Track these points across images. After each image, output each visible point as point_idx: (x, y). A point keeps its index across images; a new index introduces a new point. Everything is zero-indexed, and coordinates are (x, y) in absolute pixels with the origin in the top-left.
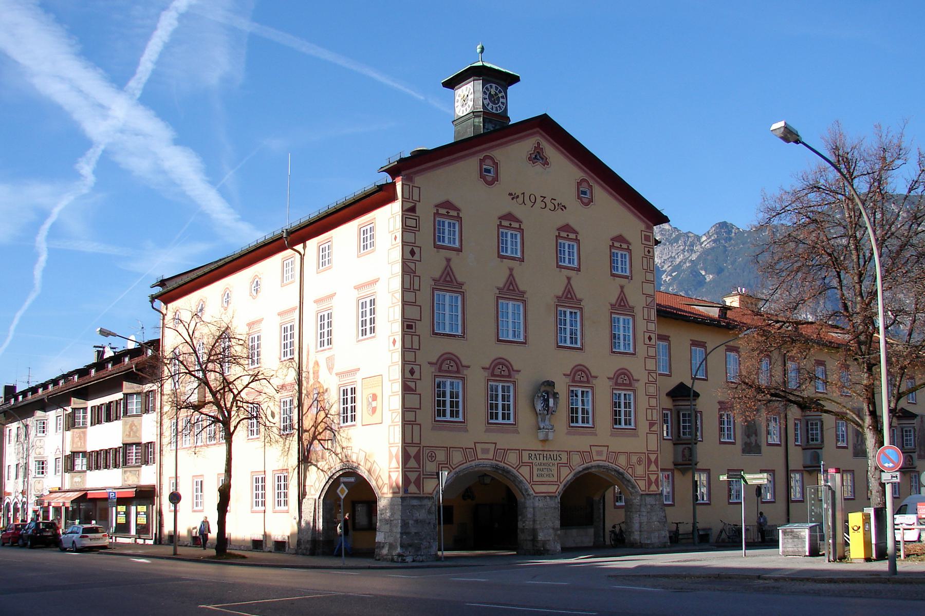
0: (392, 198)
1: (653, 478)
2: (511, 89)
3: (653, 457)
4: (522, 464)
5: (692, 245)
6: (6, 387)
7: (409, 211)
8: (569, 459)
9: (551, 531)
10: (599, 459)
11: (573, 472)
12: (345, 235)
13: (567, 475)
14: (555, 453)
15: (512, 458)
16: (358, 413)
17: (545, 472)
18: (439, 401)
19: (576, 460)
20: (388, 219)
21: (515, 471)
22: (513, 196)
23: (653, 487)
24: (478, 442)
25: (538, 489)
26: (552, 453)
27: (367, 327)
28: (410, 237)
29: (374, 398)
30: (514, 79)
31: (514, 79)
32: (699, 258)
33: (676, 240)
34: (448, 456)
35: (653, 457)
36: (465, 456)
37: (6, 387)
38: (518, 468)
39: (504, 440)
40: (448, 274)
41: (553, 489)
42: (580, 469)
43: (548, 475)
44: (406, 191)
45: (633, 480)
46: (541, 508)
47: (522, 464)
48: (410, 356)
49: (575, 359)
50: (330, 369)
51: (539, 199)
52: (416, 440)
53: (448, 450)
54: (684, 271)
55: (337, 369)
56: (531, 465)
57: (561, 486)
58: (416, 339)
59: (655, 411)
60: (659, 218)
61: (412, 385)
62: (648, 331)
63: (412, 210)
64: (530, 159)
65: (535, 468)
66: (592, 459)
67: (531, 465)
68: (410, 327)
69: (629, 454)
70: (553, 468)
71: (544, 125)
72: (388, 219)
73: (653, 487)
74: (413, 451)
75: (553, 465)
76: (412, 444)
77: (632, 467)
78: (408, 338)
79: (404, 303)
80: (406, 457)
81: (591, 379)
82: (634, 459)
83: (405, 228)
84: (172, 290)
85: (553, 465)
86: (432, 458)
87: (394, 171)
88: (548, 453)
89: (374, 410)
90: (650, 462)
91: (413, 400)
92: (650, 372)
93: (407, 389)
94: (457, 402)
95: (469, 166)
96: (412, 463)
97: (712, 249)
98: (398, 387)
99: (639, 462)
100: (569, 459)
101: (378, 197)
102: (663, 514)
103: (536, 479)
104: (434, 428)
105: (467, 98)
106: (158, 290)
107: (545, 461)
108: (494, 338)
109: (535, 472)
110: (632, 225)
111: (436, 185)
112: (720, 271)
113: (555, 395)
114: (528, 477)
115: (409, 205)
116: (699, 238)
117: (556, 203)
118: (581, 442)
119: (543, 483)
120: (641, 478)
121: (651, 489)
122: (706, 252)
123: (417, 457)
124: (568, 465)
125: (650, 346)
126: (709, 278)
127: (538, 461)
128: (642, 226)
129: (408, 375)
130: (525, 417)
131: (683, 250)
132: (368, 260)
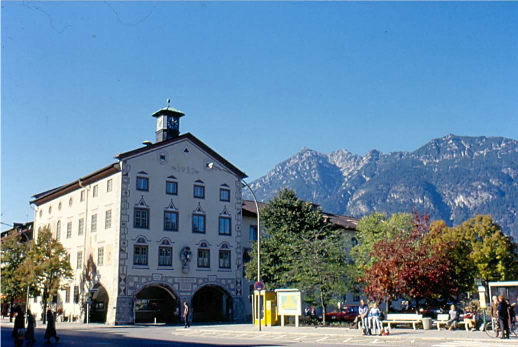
0: (117, 171)
2: (181, 119)
3: (239, 281)
5: (358, 162)
7: (125, 175)
10: (212, 281)
12: (102, 183)
13: (196, 288)
16: (104, 262)
19: (201, 281)
20: (117, 178)
22: (174, 168)
23: (239, 294)
24: (153, 273)
27: (108, 224)
28: (125, 186)
29: (110, 254)
30: (182, 115)
31: (182, 115)
32: (362, 168)
33: (350, 159)
34: (197, 281)
35: (239, 281)
39: (166, 273)
41: (189, 294)
44: (124, 167)
45: (229, 291)
48: (123, 237)
49: (199, 238)
50: (96, 240)
51: (186, 169)
54: (354, 176)
55: (98, 241)
57: (193, 294)
58: (126, 230)
59: (240, 261)
60: (242, 175)
61: (124, 249)
62: (237, 225)
63: (127, 175)
66: (208, 282)
68: (123, 224)
69: (226, 280)
71: (189, 136)
72: (117, 178)
73: (239, 294)
74: (123, 278)
76: (123, 274)
77: (229, 285)
78: (122, 229)
79: (121, 214)
80: (120, 280)
83: (123, 182)
84: (41, 199)
87: (120, 157)
89: (109, 259)
90: (237, 283)
91: (124, 256)
92: (238, 243)
93: (121, 251)
95: (154, 154)
96: (122, 282)
97: (369, 164)
98: (117, 250)
99: (232, 283)
101: (109, 171)
103: (181, 290)
105: (161, 123)
106: (34, 199)
110: (231, 179)
111: (137, 165)
112: (373, 175)
113: (190, 253)
114: (177, 289)
115: (124, 173)
116: (362, 158)
117: (194, 170)
118: (204, 274)
120: (233, 290)
122: (366, 166)
123: (125, 280)
125: (238, 231)
126: (368, 179)
128: (237, 179)
129: (122, 245)
130: (176, 262)
131: (354, 165)
132: (108, 196)
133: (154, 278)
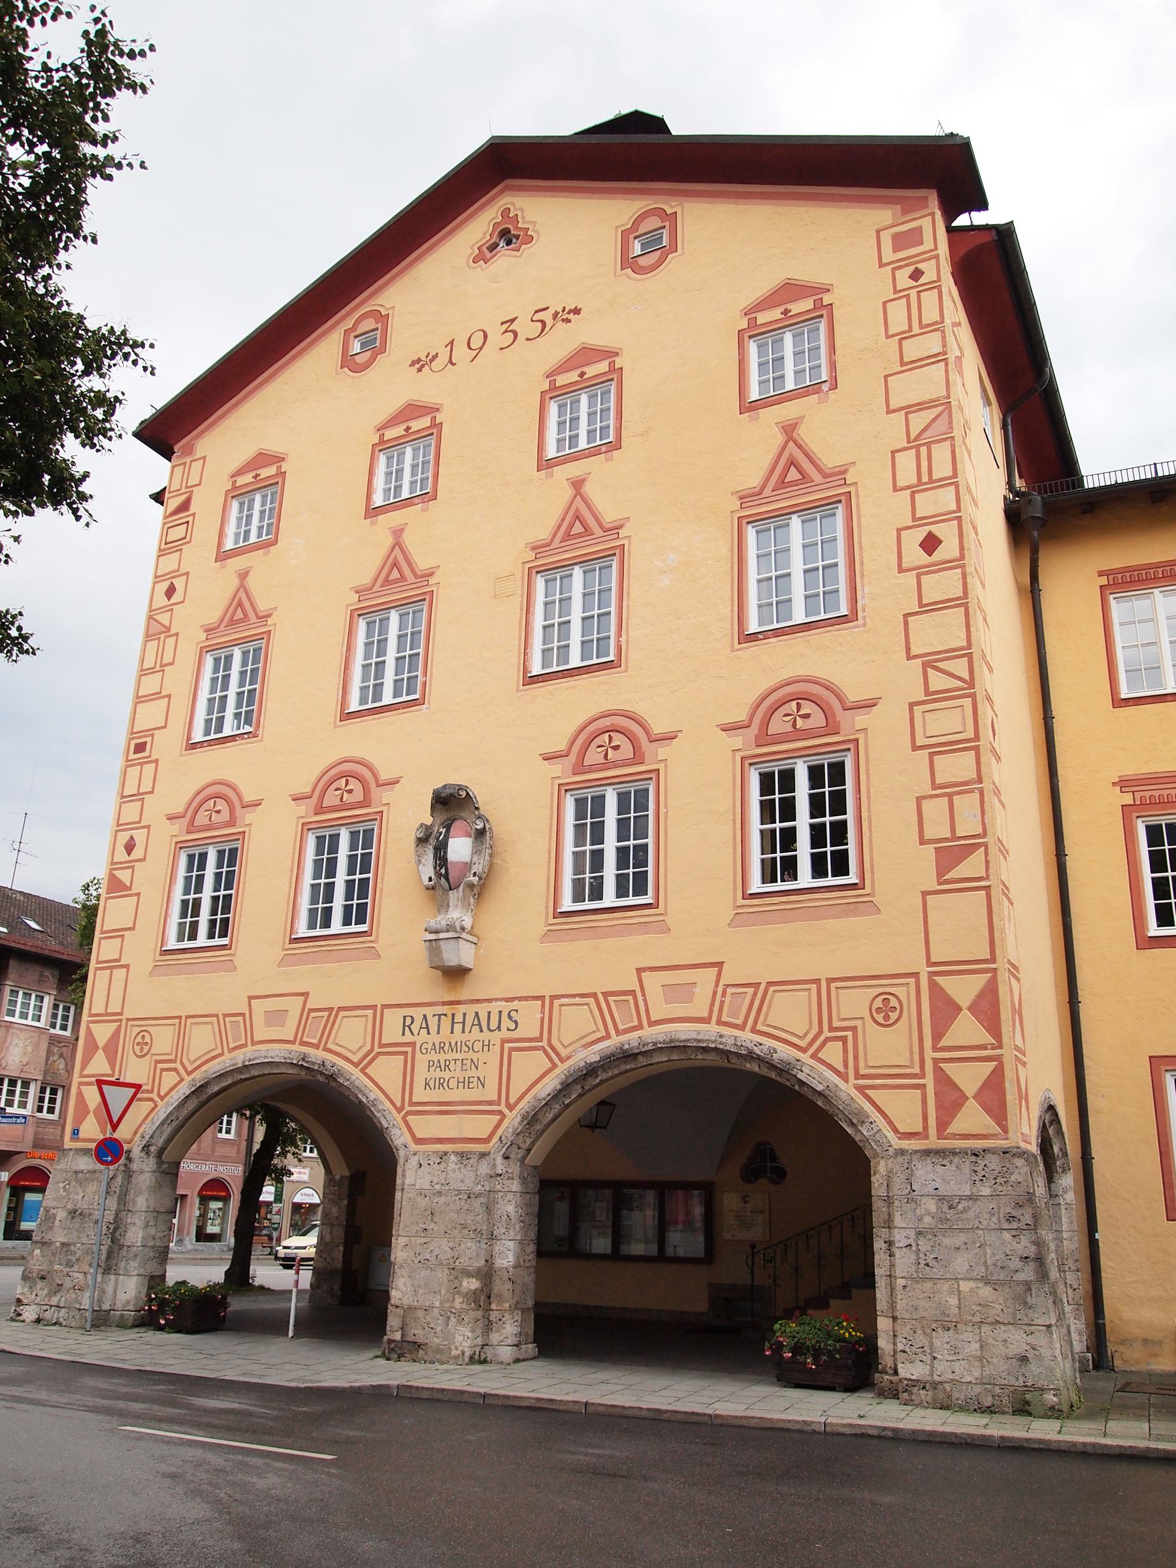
1: (969, 1077)
3: (963, 989)
4: (379, 1049)
6: (987, 209)
8: (547, 1022)
9: (442, 1275)
11: (562, 1070)
14: (494, 1007)
15: (351, 1036)
17: (456, 1072)
18: (365, 869)
21: (355, 1074)
23: (972, 1119)
25: (428, 1126)
26: (482, 1009)
35: (963, 989)
36: (222, 1035)
37: (987, 209)
38: (364, 1064)
39: (335, 981)
40: (240, 604)
41: (480, 1126)
42: (592, 1055)
43: (466, 1083)
46: (422, 1193)
47: (379, 1049)
52: (114, 1007)
53: (181, 1022)
56: (406, 1051)
64: (628, 262)
65: (421, 1061)
67: (406, 1051)
70: (483, 1056)
73: (972, 1119)
75: (487, 1046)
77: (847, 1034)
81: (841, 716)
82: (853, 1004)
85: (487, 1046)
86: (143, 1047)
88: (471, 1010)
94: (579, 840)
100: (547, 1022)
102: (1024, 1246)
103: (420, 1094)
104: (549, 936)
107: (458, 1036)
108: (901, 526)
109: (421, 1073)
118: (605, 960)
119: (445, 1109)
121: (959, 1124)
124: (543, 1043)
127: (434, 1038)
133: (259, 1020)
